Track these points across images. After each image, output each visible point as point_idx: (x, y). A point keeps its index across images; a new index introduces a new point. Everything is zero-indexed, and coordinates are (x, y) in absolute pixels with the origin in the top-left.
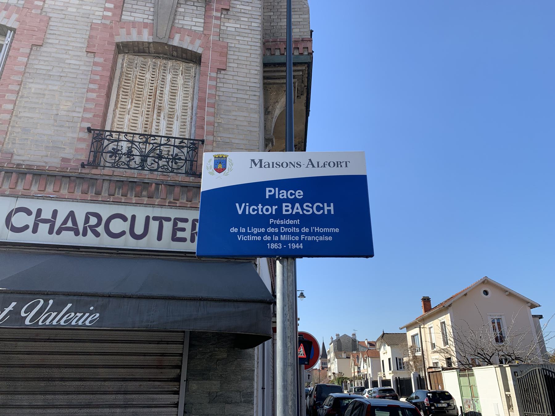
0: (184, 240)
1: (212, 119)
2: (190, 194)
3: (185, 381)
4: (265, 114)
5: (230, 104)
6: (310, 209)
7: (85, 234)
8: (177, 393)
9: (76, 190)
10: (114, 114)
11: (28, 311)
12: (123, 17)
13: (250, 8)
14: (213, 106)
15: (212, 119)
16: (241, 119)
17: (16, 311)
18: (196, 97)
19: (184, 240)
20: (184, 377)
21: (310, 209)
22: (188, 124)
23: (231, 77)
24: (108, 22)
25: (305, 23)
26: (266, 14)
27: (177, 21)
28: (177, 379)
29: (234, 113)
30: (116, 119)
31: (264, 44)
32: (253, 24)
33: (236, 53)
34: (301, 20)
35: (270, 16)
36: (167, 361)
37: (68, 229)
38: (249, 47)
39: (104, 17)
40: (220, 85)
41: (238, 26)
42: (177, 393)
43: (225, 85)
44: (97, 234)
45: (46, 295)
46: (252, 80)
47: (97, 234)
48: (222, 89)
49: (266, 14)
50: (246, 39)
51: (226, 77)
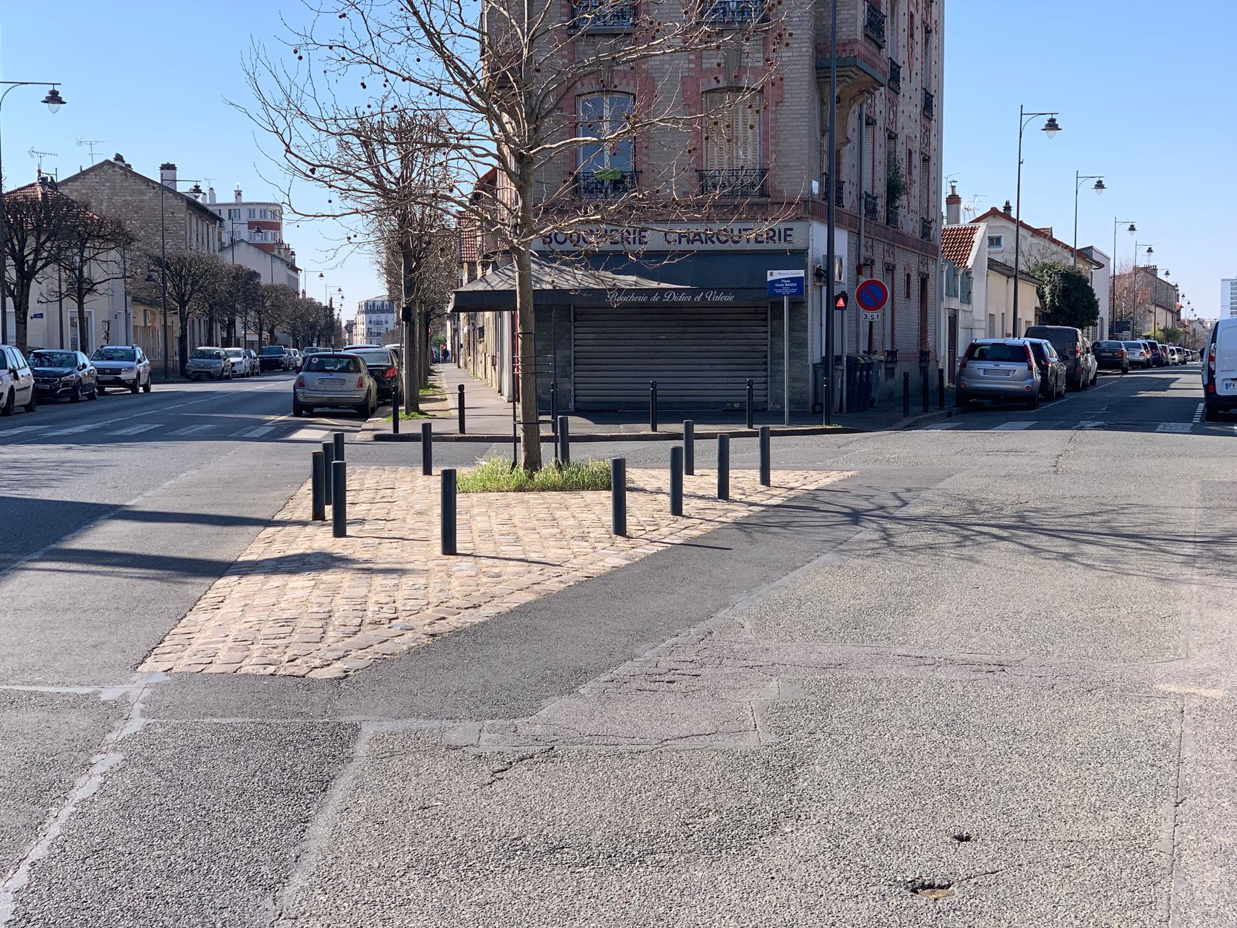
0: (762, 242)
1: (774, 148)
2: (763, 210)
3: (239, 193)
4: (821, 105)
5: (786, 132)
6: (791, 285)
7: (706, 243)
8: (766, 326)
9: (811, 386)
10: (707, 149)
11: (708, 295)
12: (704, 66)
13: (800, 32)
14: (774, 137)
15: (774, 148)
16: (795, 144)
17: (704, 296)
18: (762, 123)
19: (762, 242)
20: (769, 318)
21: (791, 285)
22: (758, 148)
23: (786, 108)
24: (693, 74)
25: (852, 20)
26: (818, 10)
27: (742, 61)
28: (766, 319)
29: (790, 140)
30: (709, 152)
31: (816, 47)
32: (803, 49)
33: (790, 84)
34: (849, 16)
35: (822, 12)
36: (760, 310)
37: (697, 240)
38: (800, 75)
39: (690, 70)
40: (778, 117)
41: (790, 54)
42: (766, 326)
43: (783, 116)
44: (713, 242)
45: (713, 289)
46: (803, 107)
47: (713, 242)
48: (781, 120)
49: (818, 10)
50: (797, 67)
51: (783, 108)
